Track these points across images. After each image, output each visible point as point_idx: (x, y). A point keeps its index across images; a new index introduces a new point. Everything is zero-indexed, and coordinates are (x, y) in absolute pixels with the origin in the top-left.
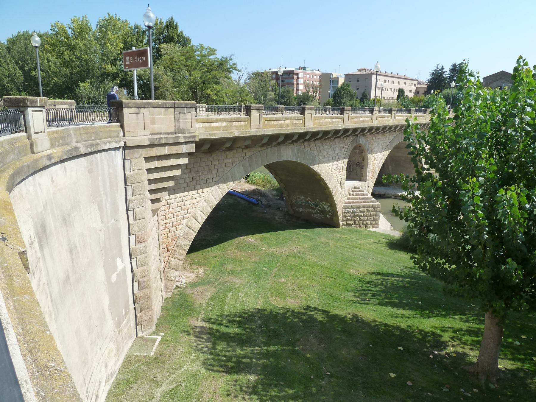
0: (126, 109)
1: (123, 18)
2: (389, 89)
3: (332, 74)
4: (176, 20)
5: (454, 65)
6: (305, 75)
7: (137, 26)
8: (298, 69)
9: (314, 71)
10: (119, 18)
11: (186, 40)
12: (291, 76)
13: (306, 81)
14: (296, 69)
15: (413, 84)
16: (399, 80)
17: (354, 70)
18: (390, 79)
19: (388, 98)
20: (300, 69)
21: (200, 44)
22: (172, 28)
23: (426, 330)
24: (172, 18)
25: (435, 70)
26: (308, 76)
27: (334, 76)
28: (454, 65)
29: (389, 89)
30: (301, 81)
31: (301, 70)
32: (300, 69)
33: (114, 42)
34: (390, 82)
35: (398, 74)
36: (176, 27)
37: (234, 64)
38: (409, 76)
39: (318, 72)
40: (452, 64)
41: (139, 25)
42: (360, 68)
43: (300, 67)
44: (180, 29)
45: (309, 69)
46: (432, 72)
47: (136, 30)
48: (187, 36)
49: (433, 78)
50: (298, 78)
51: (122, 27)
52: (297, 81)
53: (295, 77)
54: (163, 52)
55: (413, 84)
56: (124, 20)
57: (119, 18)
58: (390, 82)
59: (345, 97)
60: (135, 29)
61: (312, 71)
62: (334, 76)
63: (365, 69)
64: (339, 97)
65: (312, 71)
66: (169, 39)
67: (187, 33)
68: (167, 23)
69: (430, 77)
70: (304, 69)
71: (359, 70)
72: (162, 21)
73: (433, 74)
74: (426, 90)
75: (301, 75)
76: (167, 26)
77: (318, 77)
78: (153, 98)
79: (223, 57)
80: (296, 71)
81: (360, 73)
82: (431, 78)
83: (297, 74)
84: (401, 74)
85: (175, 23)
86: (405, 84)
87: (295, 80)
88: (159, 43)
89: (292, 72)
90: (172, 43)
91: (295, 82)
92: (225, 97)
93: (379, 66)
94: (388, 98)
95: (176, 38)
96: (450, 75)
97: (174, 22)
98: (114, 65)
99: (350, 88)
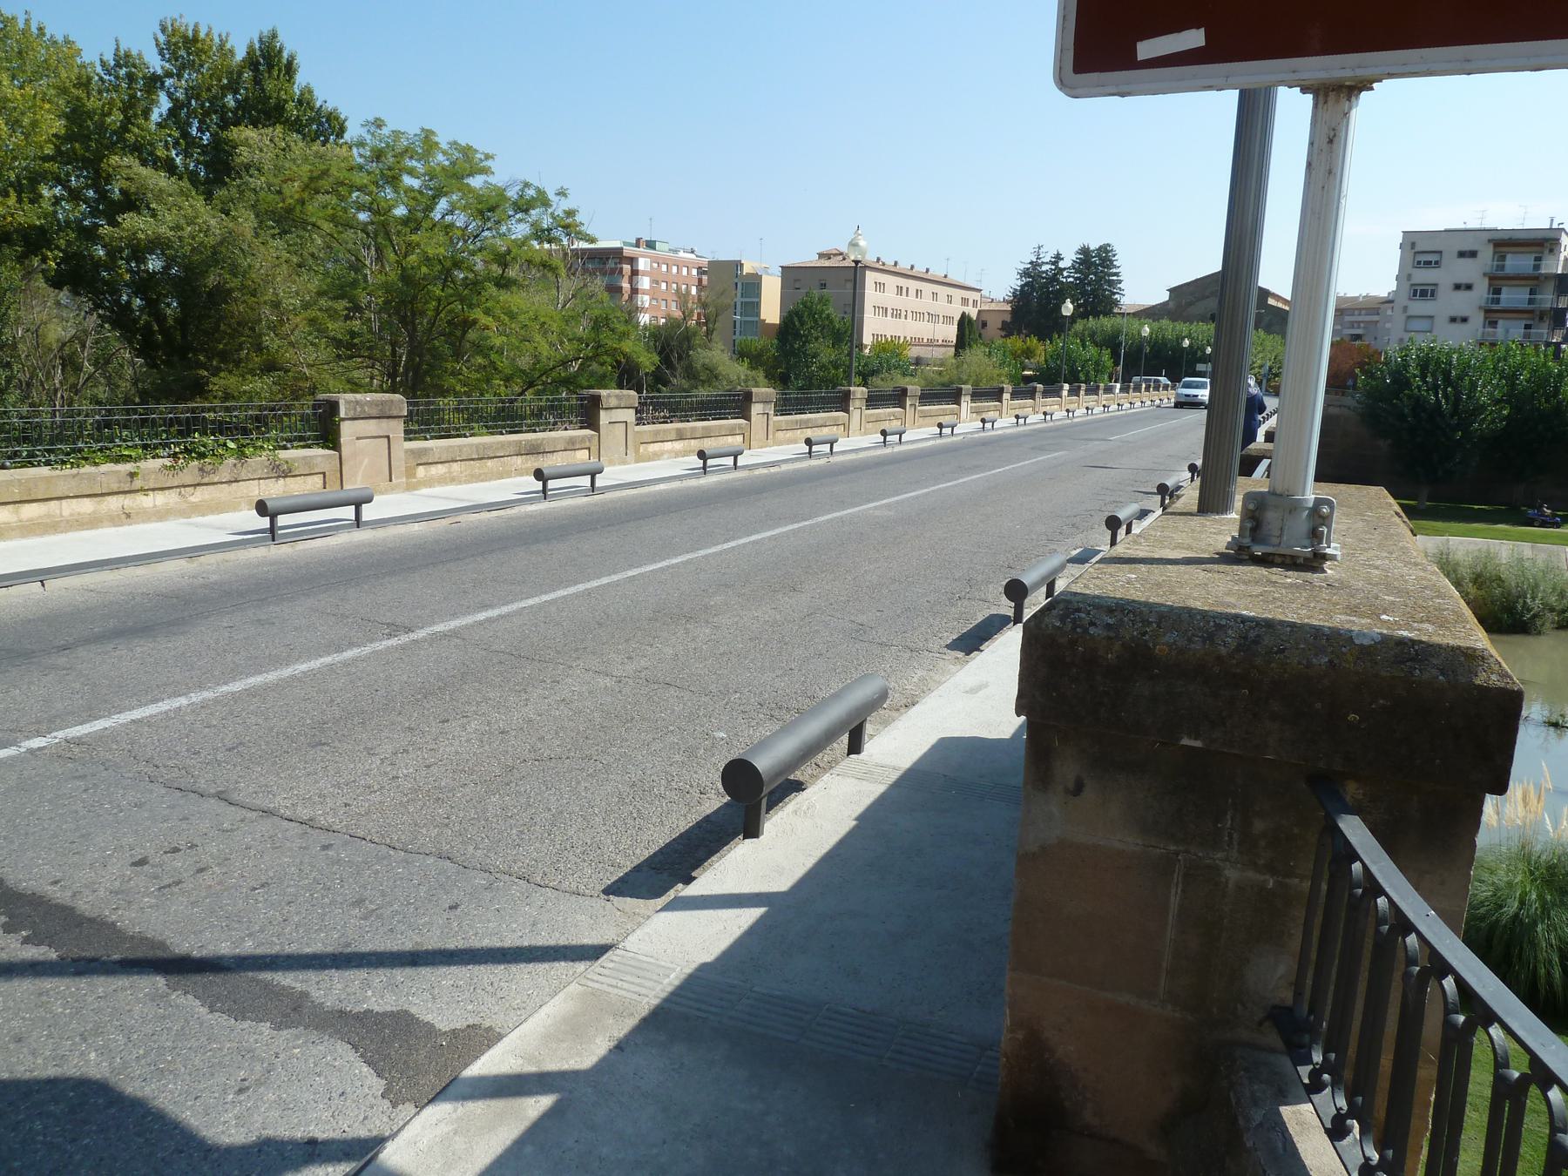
0: (347, 422)
1: (55, 30)
2: (910, 314)
3: (742, 265)
4: (289, 44)
5: (1085, 251)
6: (655, 265)
7: (127, 55)
8: (631, 245)
9: (681, 254)
10: (40, 29)
11: (328, 120)
12: (611, 264)
13: (657, 282)
14: (625, 243)
15: (971, 302)
16: (950, 291)
17: (805, 255)
18: (913, 285)
19: (925, 341)
20: (637, 244)
21: (423, 130)
22: (275, 73)
23: (88, 512)
24: (274, 36)
25: (1031, 263)
26: (664, 268)
27: (747, 269)
28: (1085, 251)
29: (910, 314)
30: (644, 283)
31: (641, 249)
32: (637, 244)
33: (23, 114)
34: (912, 292)
35: (927, 270)
36: (290, 69)
37: (570, 213)
38: (954, 277)
39: (693, 256)
40: (1077, 247)
41: (134, 53)
42: (824, 249)
43: (638, 240)
44: (301, 79)
45: (665, 247)
46: (1022, 267)
47: (123, 72)
48: (330, 106)
49: (1026, 284)
50: (635, 273)
51: (53, 62)
52: (631, 282)
53: (627, 268)
54: (244, 156)
55: (971, 302)
56: (60, 39)
57: (40, 29)
58: (912, 292)
59: (817, 339)
60: (118, 65)
61: (676, 251)
62: (747, 269)
63: (841, 254)
64: (797, 336)
65: (676, 251)
66: (265, 111)
67: (328, 96)
68: (251, 51)
69: (1019, 283)
70: (651, 245)
71: (821, 256)
72: (228, 46)
73: (1026, 273)
74: (1008, 318)
75: (642, 264)
76: (251, 62)
77: (694, 272)
78: (974, 405)
79: (527, 185)
80: (629, 251)
81: (827, 263)
82: (1022, 286)
83: (632, 261)
84: (937, 272)
85: (285, 55)
86: (950, 299)
87: (626, 278)
88: (225, 124)
89: (617, 254)
90: (279, 128)
91: (626, 285)
92: (538, 338)
93: (862, 243)
94: (925, 341)
95: (292, 110)
96: (1076, 279)
97: (280, 51)
98: (32, 202)
99: (831, 310)
